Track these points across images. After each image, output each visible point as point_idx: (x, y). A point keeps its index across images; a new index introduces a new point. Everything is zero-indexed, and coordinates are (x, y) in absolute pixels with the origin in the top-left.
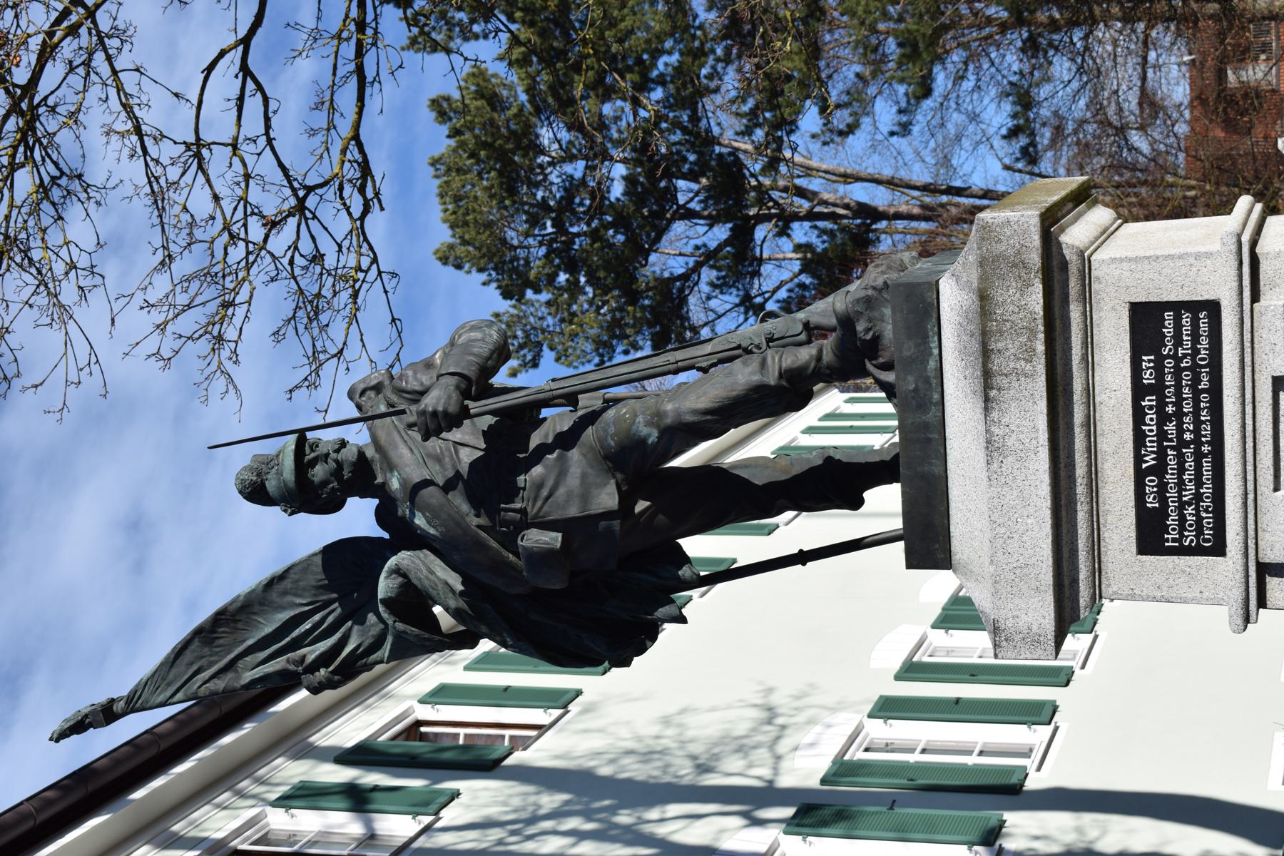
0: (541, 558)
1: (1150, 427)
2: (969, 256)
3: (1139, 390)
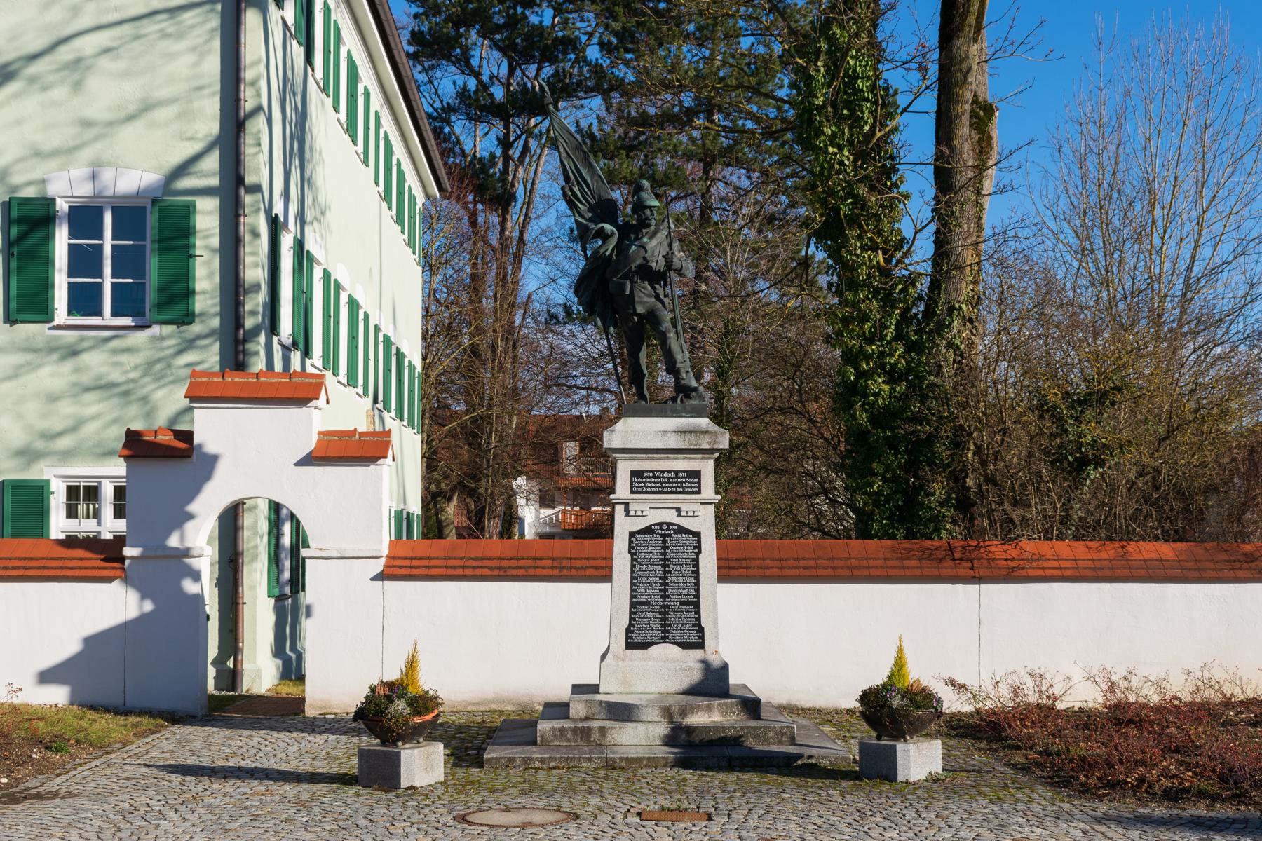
0: (623, 286)
1: (666, 475)
2: (716, 428)
3: (676, 472)
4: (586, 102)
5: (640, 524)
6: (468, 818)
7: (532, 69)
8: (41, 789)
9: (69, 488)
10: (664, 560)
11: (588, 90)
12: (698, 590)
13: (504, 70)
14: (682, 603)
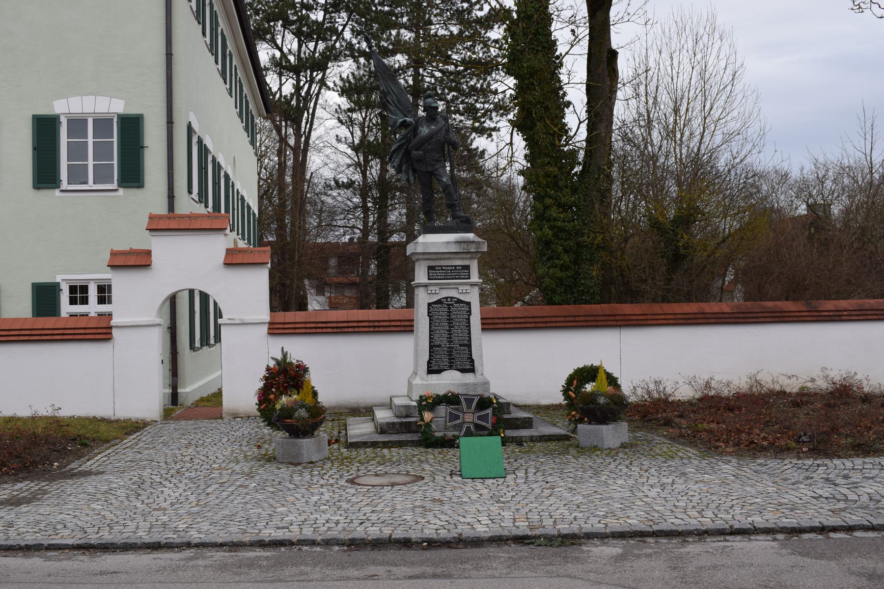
2: (480, 240)
3: (455, 266)
4: (343, 63)
5: (435, 299)
6: (356, 481)
7: (311, 45)
8: (80, 469)
9: (71, 287)
10: (449, 320)
11: (346, 56)
12: (470, 337)
13: (295, 45)
14: (461, 345)
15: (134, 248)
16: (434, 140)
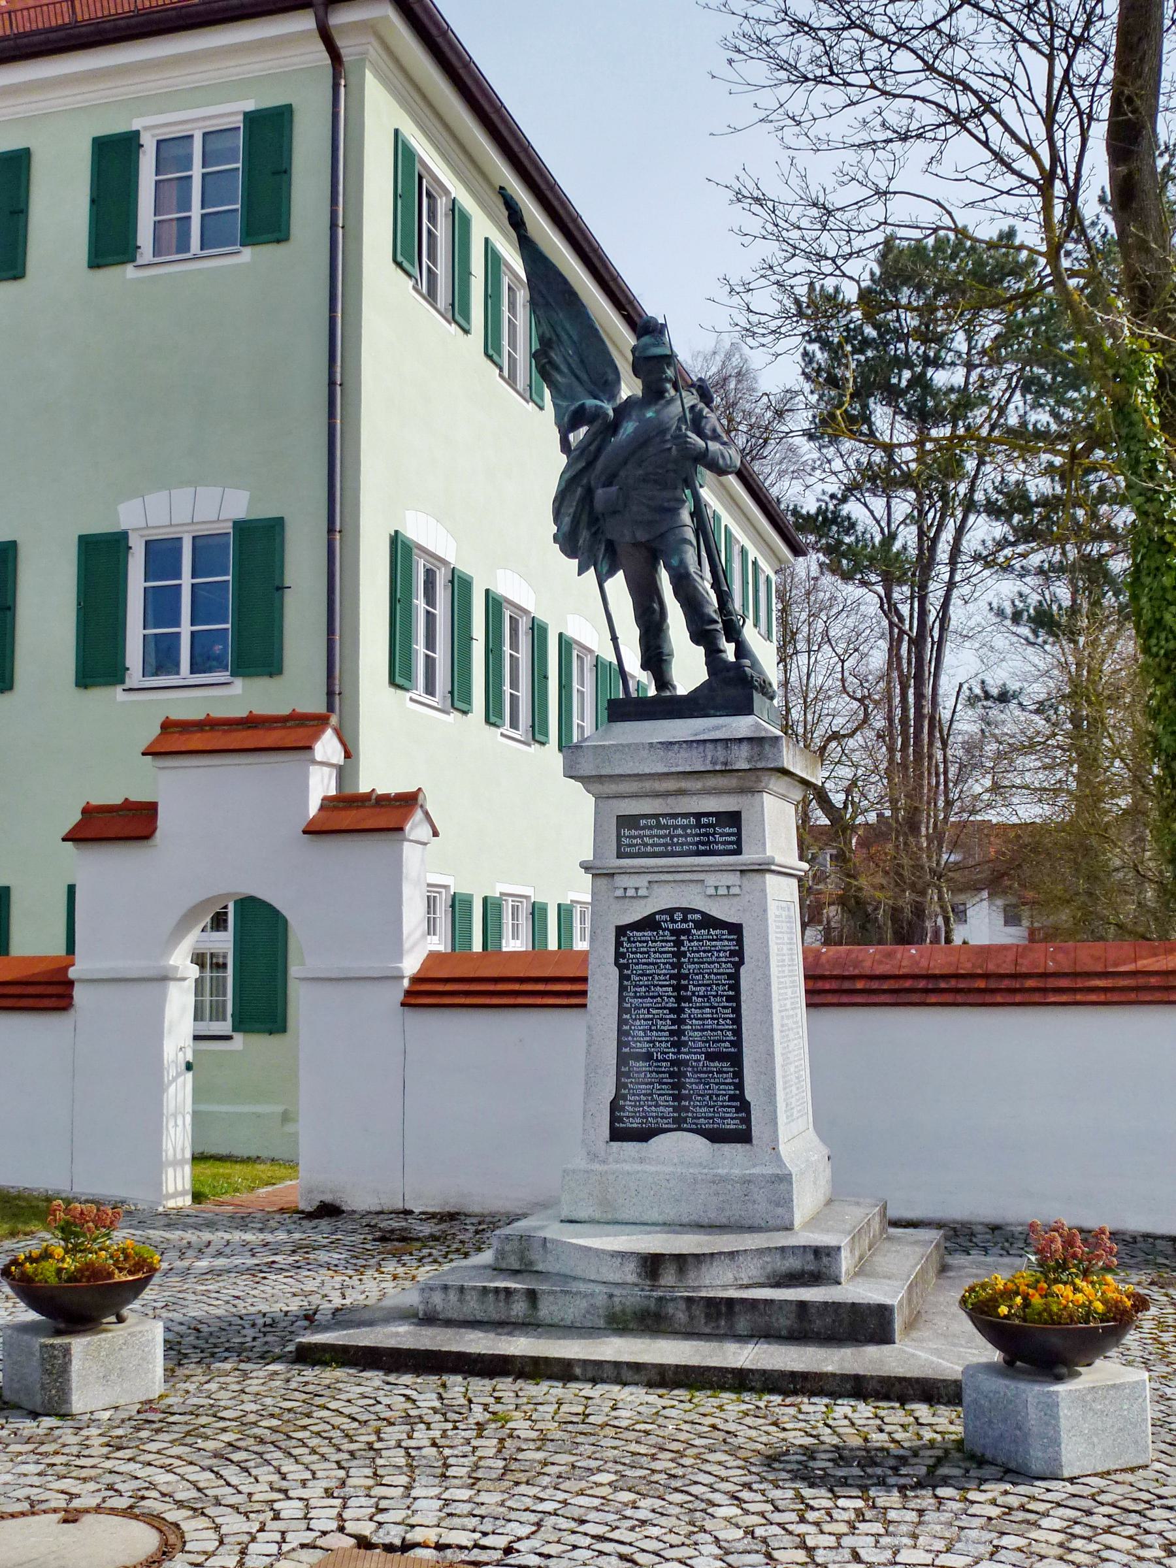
10: (679, 977)
12: (738, 1033)
14: (711, 1057)
15: (133, 799)
16: (652, 450)
